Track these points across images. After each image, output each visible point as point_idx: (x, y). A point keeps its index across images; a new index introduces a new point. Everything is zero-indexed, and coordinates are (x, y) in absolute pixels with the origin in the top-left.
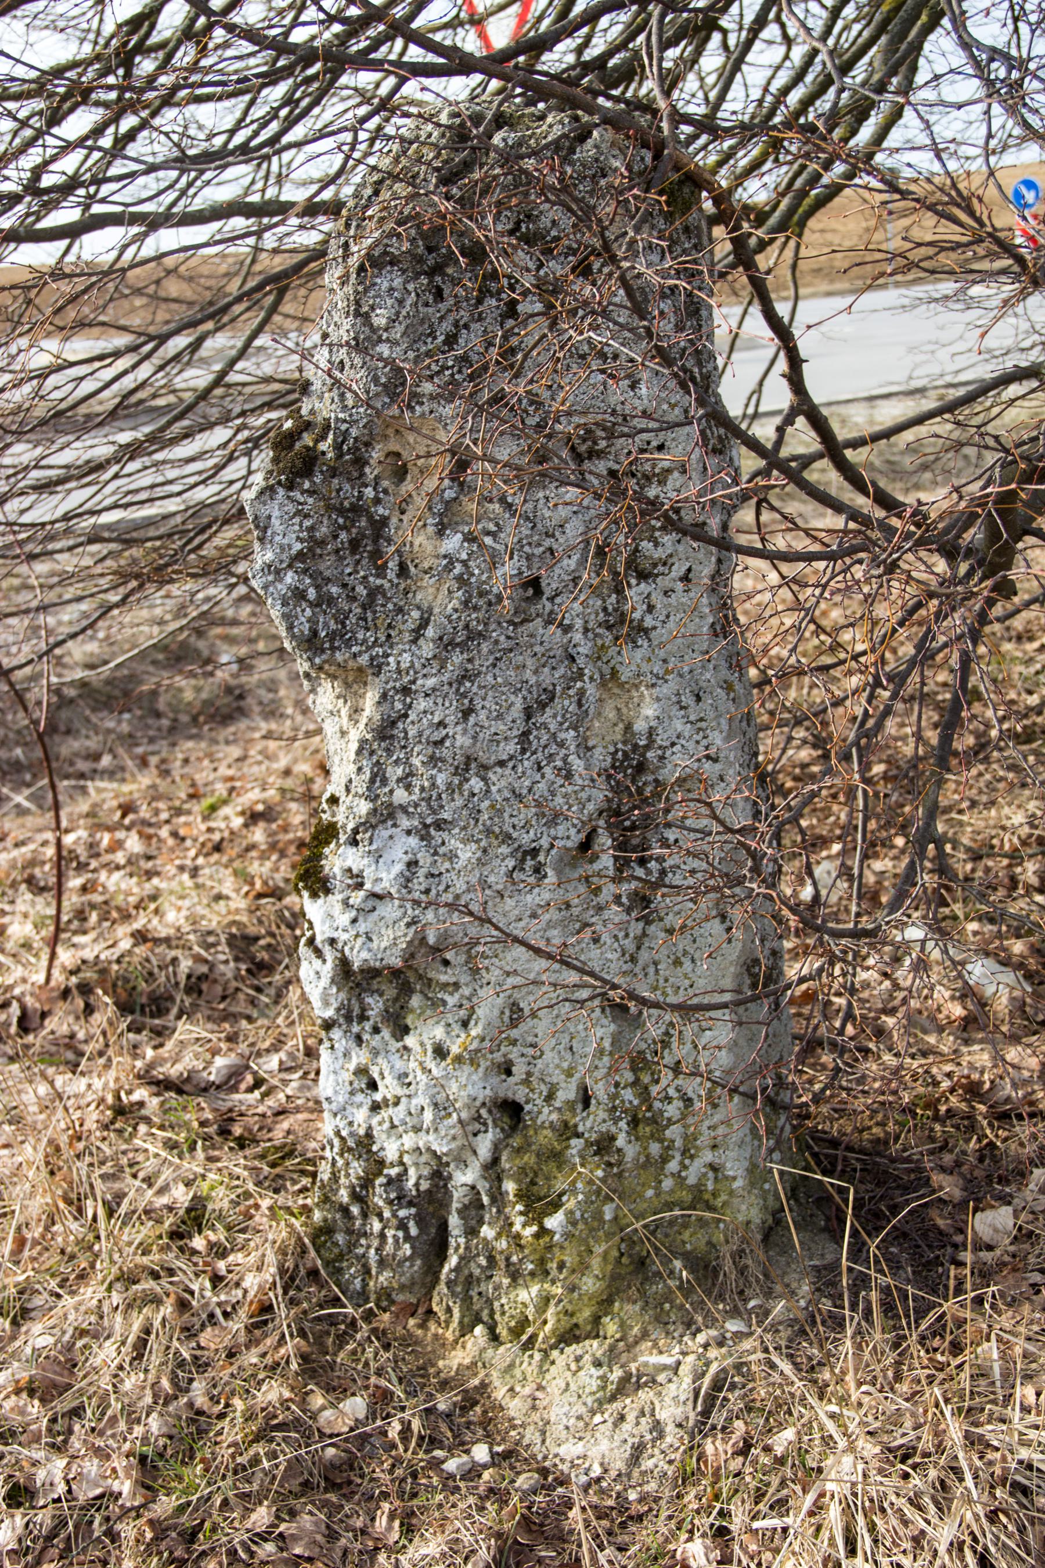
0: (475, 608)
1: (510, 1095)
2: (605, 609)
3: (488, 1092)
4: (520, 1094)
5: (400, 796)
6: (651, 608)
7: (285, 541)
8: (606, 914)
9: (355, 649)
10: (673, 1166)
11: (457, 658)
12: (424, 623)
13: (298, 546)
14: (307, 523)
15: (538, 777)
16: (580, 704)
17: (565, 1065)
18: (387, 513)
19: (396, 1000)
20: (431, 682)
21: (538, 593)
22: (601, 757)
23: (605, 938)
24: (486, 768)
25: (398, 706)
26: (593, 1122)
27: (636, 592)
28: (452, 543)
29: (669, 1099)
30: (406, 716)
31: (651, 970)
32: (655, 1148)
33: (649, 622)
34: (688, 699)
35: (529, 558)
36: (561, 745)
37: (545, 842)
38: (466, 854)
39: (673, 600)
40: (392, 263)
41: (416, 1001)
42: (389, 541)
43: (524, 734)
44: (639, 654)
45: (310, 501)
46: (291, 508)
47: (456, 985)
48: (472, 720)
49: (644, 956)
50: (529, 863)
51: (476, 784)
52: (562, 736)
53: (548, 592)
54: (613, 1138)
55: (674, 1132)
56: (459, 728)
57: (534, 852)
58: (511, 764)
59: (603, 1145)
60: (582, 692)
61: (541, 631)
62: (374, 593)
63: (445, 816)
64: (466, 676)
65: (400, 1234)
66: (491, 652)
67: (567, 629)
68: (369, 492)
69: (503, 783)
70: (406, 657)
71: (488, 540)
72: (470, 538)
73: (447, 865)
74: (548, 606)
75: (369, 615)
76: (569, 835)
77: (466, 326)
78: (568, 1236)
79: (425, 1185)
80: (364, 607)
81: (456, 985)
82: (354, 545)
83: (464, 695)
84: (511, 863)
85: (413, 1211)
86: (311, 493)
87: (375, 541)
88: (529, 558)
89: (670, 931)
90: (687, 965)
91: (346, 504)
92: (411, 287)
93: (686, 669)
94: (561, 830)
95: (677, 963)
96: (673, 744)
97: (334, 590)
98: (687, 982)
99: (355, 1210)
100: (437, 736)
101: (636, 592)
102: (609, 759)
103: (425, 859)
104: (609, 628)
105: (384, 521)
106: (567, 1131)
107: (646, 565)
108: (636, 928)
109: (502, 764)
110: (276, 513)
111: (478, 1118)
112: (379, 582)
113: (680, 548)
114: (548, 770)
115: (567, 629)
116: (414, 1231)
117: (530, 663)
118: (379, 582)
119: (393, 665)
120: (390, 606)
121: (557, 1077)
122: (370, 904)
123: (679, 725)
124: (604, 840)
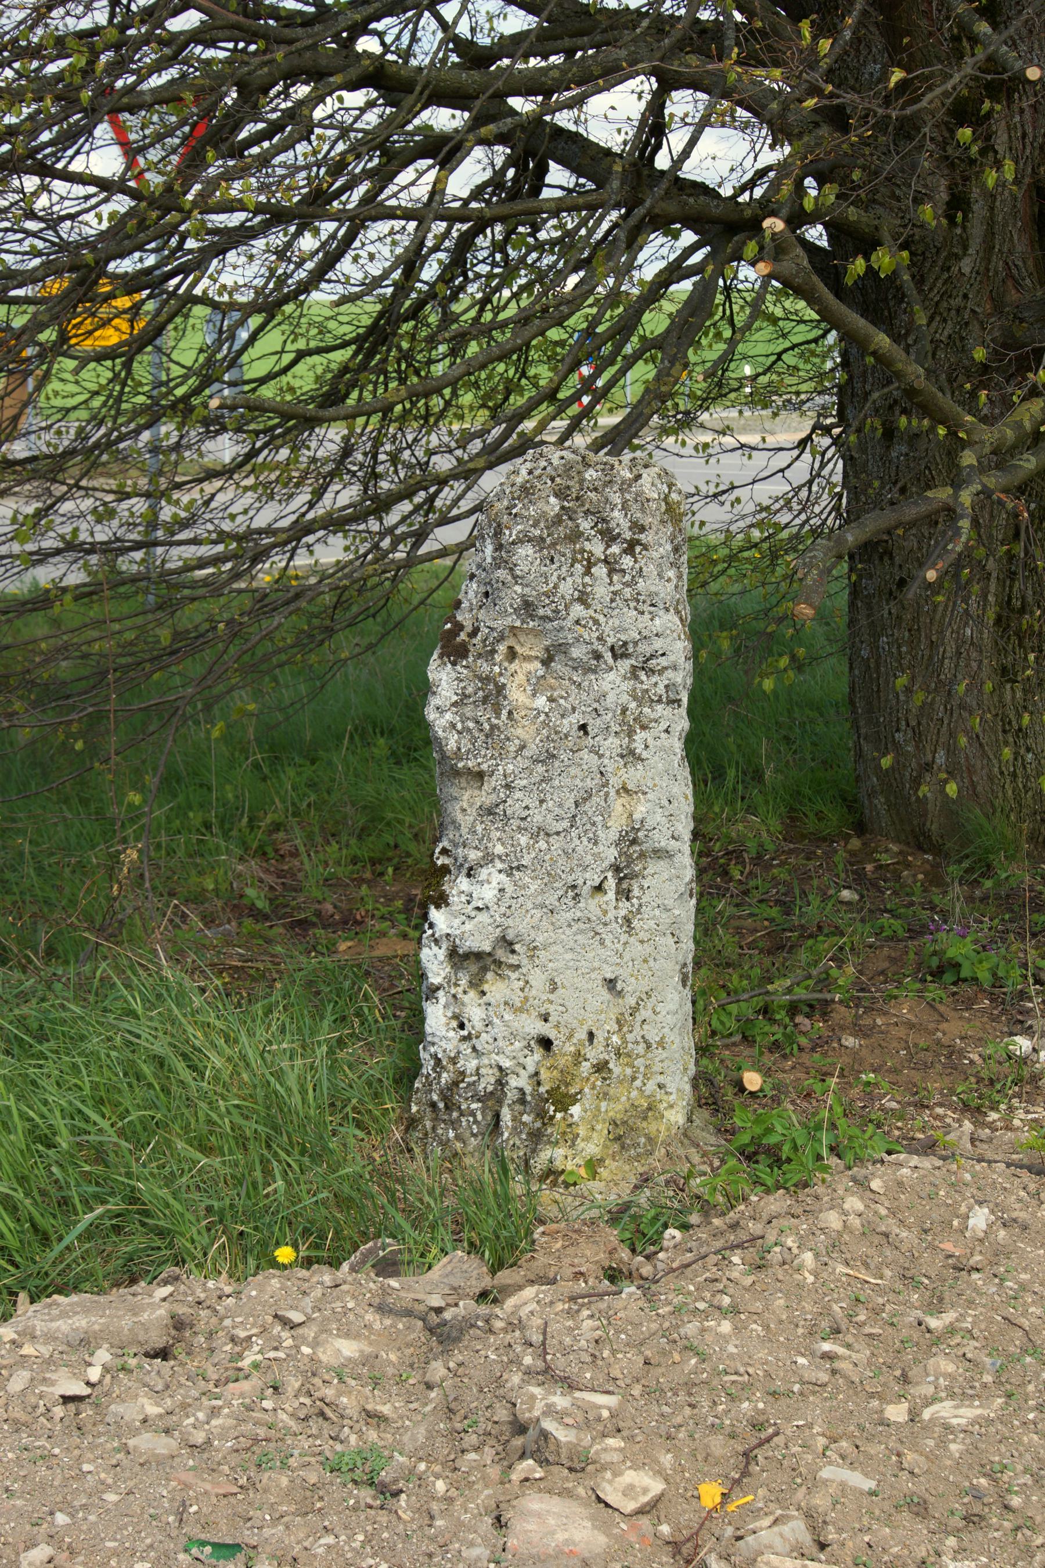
4: (552, 1035)
5: (499, 849)
10: (638, 1083)
11: (540, 769)
13: (455, 698)
20: (524, 782)
21: (586, 733)
22: (613, 835)
23: (608, 943)
24: (548, 835)
26: (594, 1054)
27: (640, 736)
28: (541, 702)
29: (637, 1043)
32: (629, 1071)
36: (594, 824)
37: (580, 882)
41: (490, 976)
44: (639, 774)
46: (454, 675)
47: (518, 967)
51: (542, 845)
53: (592, 734)
54: (607, 1062)
57: (574, 887)
59: (601, 1067)
60: (607, 794)
62: (493, 727)
67: (601, 756)
68: (497, 669)
72: (551, 700)
78: (582, 1118)
79: (490, 1088)
81: (518, 967)
82: (485, 700)
84: (560, 893)
89: (642, 942)
90: (652, 963)
94: (588, 875)
99: (441, 1105)
101: (640, 736)
103: (510, 889)
106: (578, 1057)
107: (645, 721)
109: (558, 833)
114: (585, 839)
115: (601, 756)
116: (479, 1117)
117: (580, 774)
121: (575, 1024)
123: (658, 817)
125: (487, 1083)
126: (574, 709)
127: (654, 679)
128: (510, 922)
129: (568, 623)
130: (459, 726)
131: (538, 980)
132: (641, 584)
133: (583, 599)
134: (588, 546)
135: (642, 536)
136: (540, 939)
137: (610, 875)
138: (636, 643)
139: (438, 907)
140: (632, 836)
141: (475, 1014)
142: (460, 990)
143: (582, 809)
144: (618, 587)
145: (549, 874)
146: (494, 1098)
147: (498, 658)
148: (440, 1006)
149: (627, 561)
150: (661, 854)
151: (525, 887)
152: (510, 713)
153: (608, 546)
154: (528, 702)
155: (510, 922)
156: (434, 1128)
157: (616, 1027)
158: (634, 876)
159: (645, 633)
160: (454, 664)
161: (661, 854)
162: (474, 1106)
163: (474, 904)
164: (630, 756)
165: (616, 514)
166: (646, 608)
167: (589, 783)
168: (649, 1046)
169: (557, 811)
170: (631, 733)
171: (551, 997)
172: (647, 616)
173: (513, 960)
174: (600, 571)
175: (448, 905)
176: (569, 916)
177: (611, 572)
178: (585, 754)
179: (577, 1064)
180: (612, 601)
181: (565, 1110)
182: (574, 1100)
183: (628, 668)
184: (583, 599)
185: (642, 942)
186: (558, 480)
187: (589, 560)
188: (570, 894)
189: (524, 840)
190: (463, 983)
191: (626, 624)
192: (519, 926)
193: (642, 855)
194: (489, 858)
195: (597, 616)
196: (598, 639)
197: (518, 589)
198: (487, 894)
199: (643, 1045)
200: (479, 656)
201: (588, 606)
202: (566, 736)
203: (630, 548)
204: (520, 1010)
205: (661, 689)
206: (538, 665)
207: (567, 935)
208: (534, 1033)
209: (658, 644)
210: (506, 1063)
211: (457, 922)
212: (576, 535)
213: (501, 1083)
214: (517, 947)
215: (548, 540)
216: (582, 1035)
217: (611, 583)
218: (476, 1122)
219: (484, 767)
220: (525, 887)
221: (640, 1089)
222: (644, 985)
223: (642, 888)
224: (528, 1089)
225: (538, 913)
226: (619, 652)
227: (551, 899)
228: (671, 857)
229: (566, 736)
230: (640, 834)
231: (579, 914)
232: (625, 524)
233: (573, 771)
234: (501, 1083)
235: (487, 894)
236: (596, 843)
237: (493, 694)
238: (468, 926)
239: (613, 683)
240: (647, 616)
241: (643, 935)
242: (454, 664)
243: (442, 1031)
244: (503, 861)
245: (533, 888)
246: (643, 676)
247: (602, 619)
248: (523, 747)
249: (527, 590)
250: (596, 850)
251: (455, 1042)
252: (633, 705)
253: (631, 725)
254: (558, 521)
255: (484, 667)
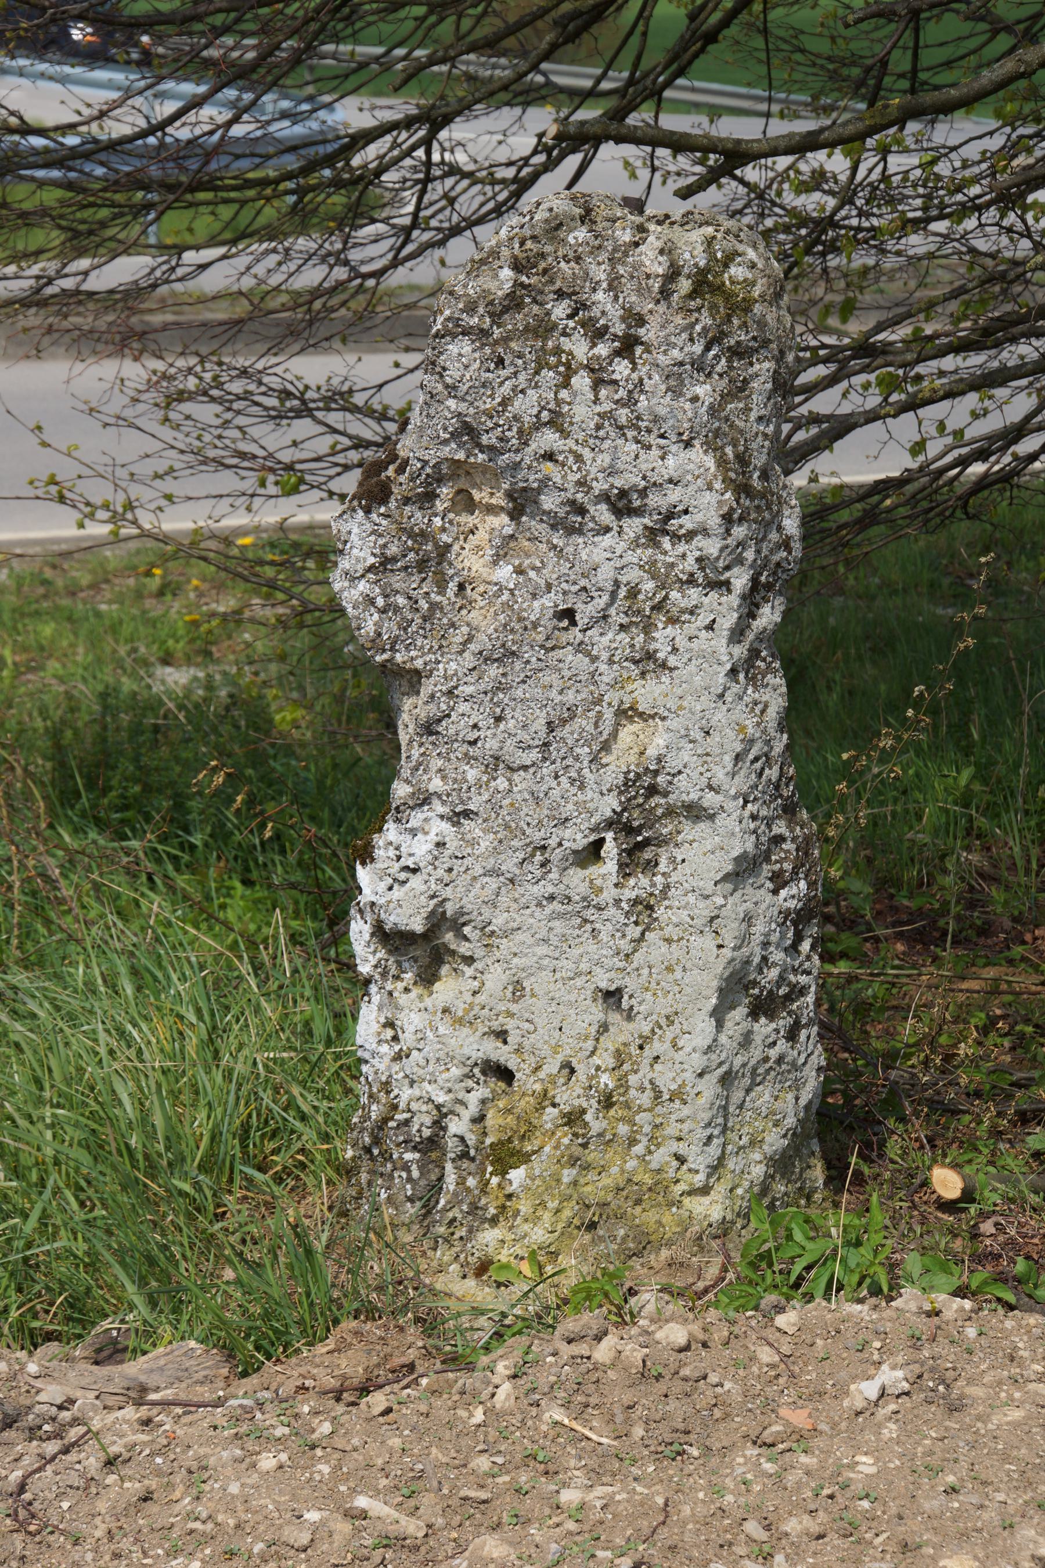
0: (512, 630)
1: (502, 1060)
2: (633, 646)
3: (480, 1054)
5: (436, 784)
6: (675, 650)
7: (362, 554)
8: (606, 914)
9: (413, 653)
10: (639, 1149)
11: (493, 671)
12: (470, 639)
13: (372, 560)
14: (381, 541)
15: (554, 784)
16: (596, 725)
17: (553, 1042)
18: (450, 540)
19: (429, 967)
20: (469, 690)
21: (573, 623)
23: (604, 936)
25: (443, 707)
26: (568, 1097)
28: (504, 573)
30: (449, 716)
31: (645, 971)
32: (623, 1129)
33: (672, 661)
34: (698, 735)
35: (565, 593)
36: (577, 758)
37: (553, 842)
38: (486, 843)
39: (695, 645)
40: (463, 334)
42: (450, 564)
43: (545, 744)
45: (384, 522)
46: (369, 527)
48: (502, 726)
49: (638, 958)
50: (538, 858)
51: (502, 783)
52: (578, 750)
54: (584, 1111)
55: (641, 1118)
56: (489, 733)
58: (532, 770)
59: (573, 1118)
60: (600, 715)
61: (570, 658)
62: (434, 606)
63: (472, 807)
64: (499, 688)
65: (404, 1175)
66: (523, 670)
67: (594, 659)
68: (438, 521)
69: (524, 785)
70: (453, 666)
71: (532, 574)
72: (519, 571)
73: (469, 850)
74: (580, 636)
75: (428, 626)
76: (578, 838)
77: (522, 391)
79: (427, 1133)
80: (425, 619)
82: (422, 565)
83: (497, 704)
84: (521, 855)
85: (417, 1155)
86: (386, 516)
87: (439, 563)
88: (565, 593)
89: (669, 941)
90: (678, 974)
91: (416, 529)
92: (477, 355)
93: (699, 708)
94: (568, 833)
95: (670, 969)
96: (680, 772)
97: (401, 601)
98: (677, 989)
100: (473, 735)
102: (621, 776)
104: (636, 662)
105: (448, 547)
106: (545, 1099)
108: (635, 932)
109: (525, 768)
110: (355, 530)
111: (469, 1076)
112: (439, 598)
113: (706, 600)
114: (564, 780)
115: (594, 659)
116: (415, 1174)
117: (557, 684)
118: (439, 598)
119: (442, 672)
120: (445, 621)
121: (546, 1051)
122: (403, 876)
123: (686, 756)
124: (610, 848)
125: (422, 1123)
126: (549, 587)
127: (682, 548)
128: (448, 892)
129: (528, 455)
130: (380, 602)
131: (496, 979)
132: (643, 402)
133: (556, 421)
134: (566, 344)
135: (642, 331)
136: (499, 921)
137: (609, 836)
138: (643, 493)
139: (363, 864)
140: (647, 780)
141: (411, 1021)
142: (400, 985)
143: (559, 733)
144: (607, 406)
145: (507, 827)
146: (431, 1146)
147: (440, 506)
148: (374, 1007)
149: (621, 368)
150: (695, 812)
151: (474, 843)
152: (461, 587)
153: (594, 345)
154: (485, 572)
155: (448, 892)
156: (370, 1183)
157: (611, 1062)
158: (662, 842)
159: (654, 478)
160: (368, 511)
161: (695, 812)
162: (408, 1156)
163: (403, 862)
164: (647, 662)
165: (600, 296)
166: (653, 439)
167: (570, 697)
168: (658, 1094)
169: (522, 735)
170: (648, 628)
171: (514, 1008)
172: (655, 452)
173: (464, 948)
174: (582, 381)
175: (373, 860)
176: (538, 890)
177: (597, 384)
178: (568, 654)
179: (540, 1108)
180: (598, 427)
181: (504, 1173)
182: (525, 1158)
183: (640, 530)
184: (556, 421)
185: (669, 941)
186: (529, 244)
187: (568, 365)
188: (538, 858)
189: (472, 774)
190: (409, 976)
191: (631, 463)
192: (460, 897)
193: (670, 812)
194: (424, 800)
195: (579, 449)
196: (580, 483)
197: (452, 403)
198: (420, 848)
199: (649, 1093)
200: (407, 501)
201: (565, 434)
202: (535, 625)
203: (627, 347)
204: (460, 1022)
205: (690, 564)
206: (505, 519)
207: (536, 919)
208: (477, 1056)
209: (674, 495)
210: (441, 1098)
211: (382, 886)
212: (543, 328)
213: (439, 1125)
214: (466, 930)
215: (497, 332)
216: (552, 1067)
217: (596, 401)
218: (410, 1179)
219: (419, 664)
220: (474, 843)
221: (642, 1158)
222: (663, 1006)
223: (672, 860)
224: (471, 1139)
225: (493, 883)
226: (622, 504)
227: (509, 864)
228: (712, 817)
229: (535, 625)
230: (659, 779)
231: (551, 889)
232: (615, 312)
233: (546, 678)
234: (439, 1125)
235: (420, 848)
236: (582, 787)
237: (432, 560)
238: (397, 893)
239: (610, 553)
240: (655, 452)
241: (669, 931)
242: (368, 511)
243: (371, 1044)
244: (444, 803)
245: (484, 844)
246: (666, 543)
247: (587, 453)
248: (470, 639)
249: (463, 407)
250: (580, 797)
251: (387, 1060)
252: (649, 586)
253: (644, 614)
254: (513, 302)
255: (418, 518)
